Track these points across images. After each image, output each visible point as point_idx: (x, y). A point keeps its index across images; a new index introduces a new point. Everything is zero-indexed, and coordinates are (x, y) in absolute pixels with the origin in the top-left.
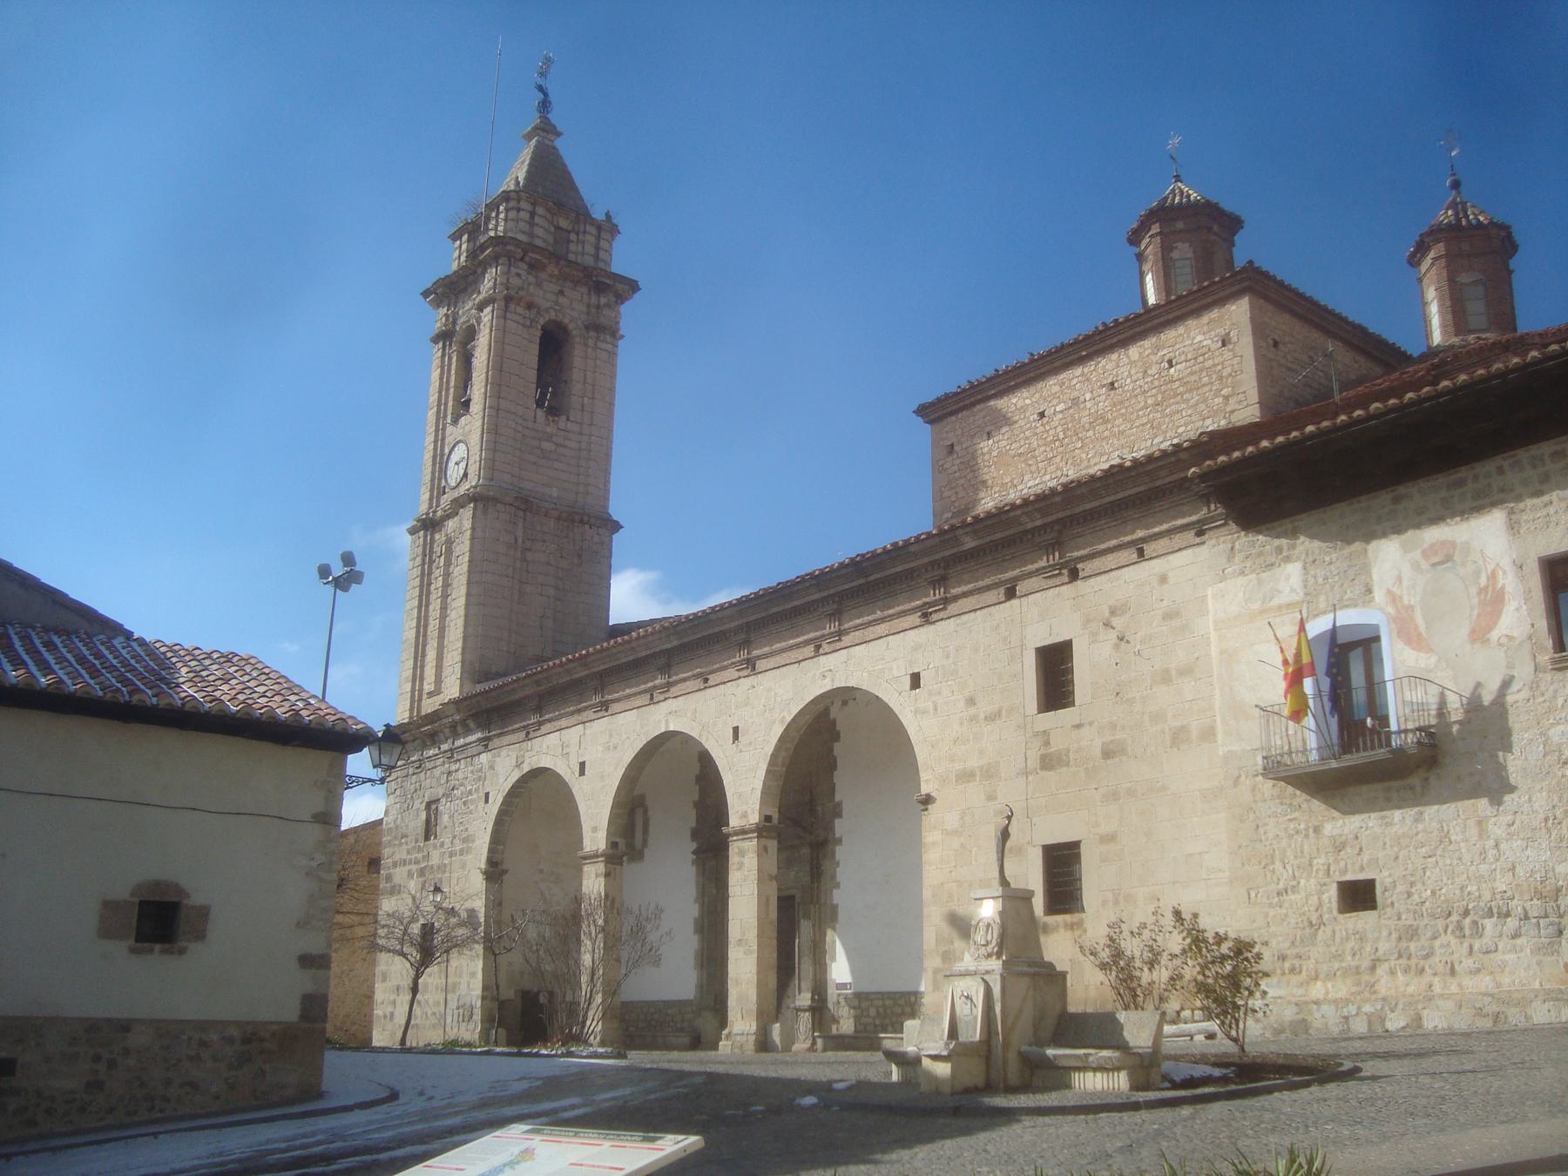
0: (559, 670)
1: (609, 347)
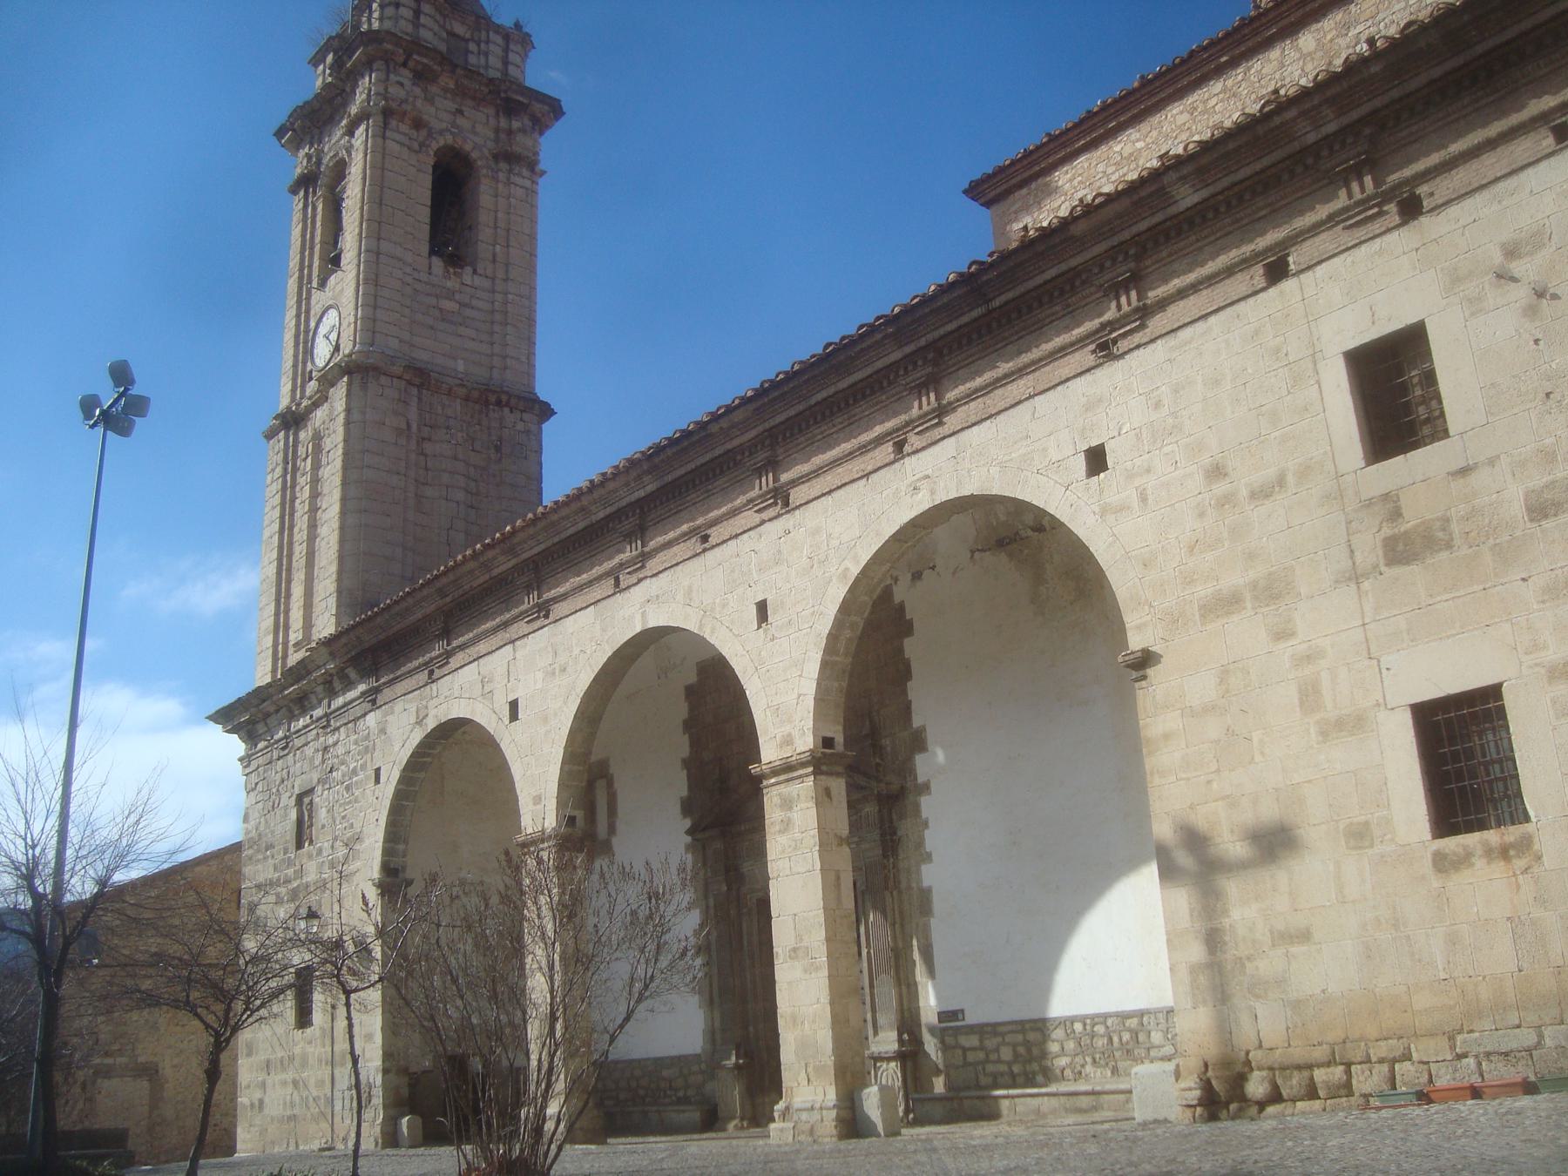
0: (472, 565)
1: (527, 183)
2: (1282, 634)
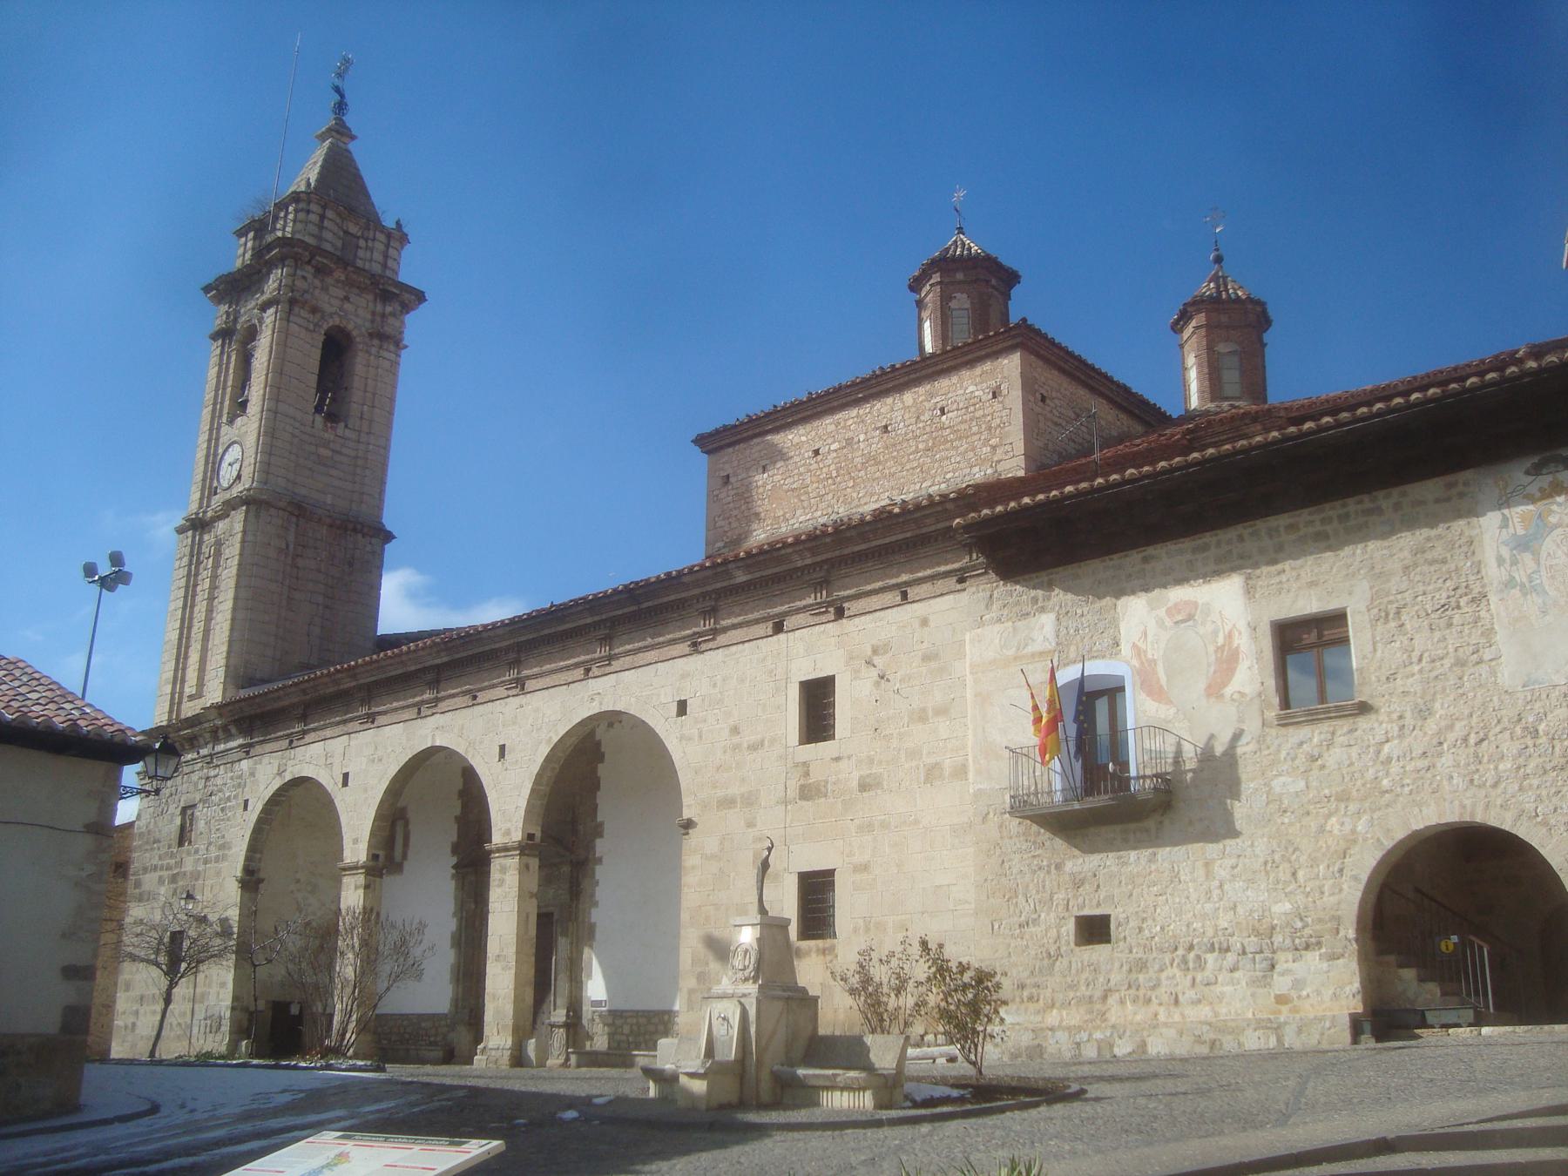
0: (326, 680)
2: (750, 825)
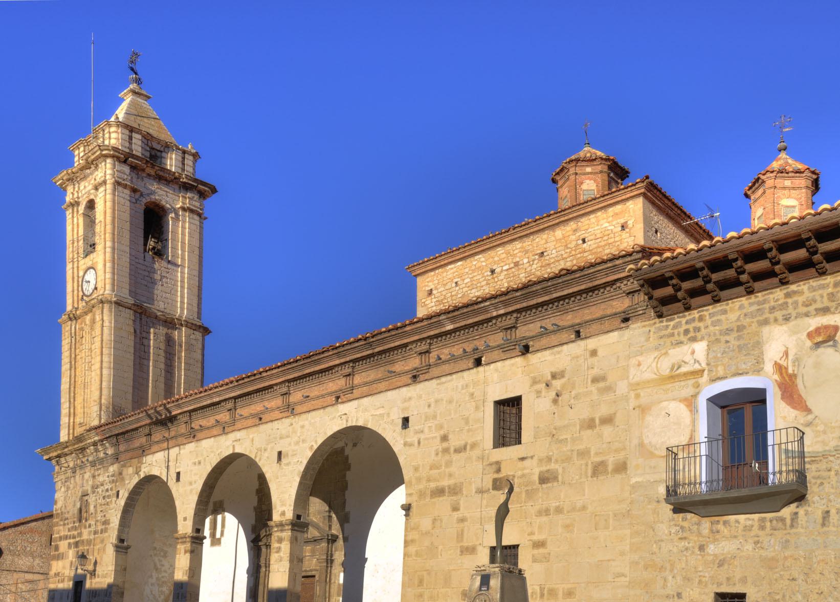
2: (455, 509)
